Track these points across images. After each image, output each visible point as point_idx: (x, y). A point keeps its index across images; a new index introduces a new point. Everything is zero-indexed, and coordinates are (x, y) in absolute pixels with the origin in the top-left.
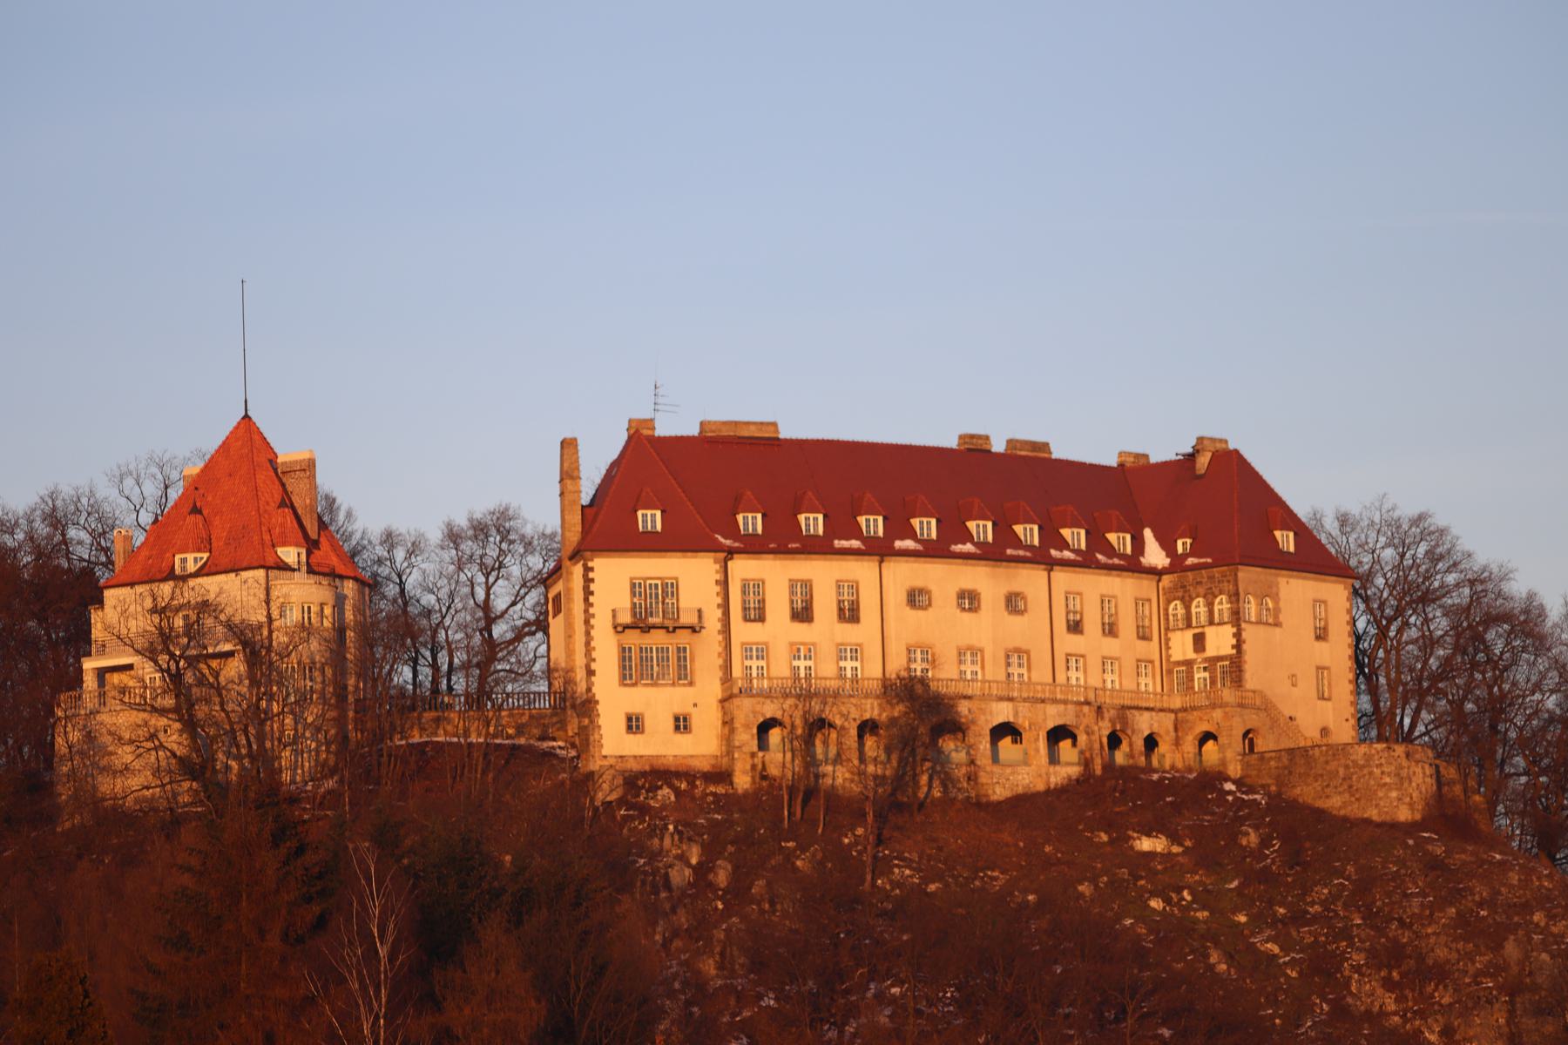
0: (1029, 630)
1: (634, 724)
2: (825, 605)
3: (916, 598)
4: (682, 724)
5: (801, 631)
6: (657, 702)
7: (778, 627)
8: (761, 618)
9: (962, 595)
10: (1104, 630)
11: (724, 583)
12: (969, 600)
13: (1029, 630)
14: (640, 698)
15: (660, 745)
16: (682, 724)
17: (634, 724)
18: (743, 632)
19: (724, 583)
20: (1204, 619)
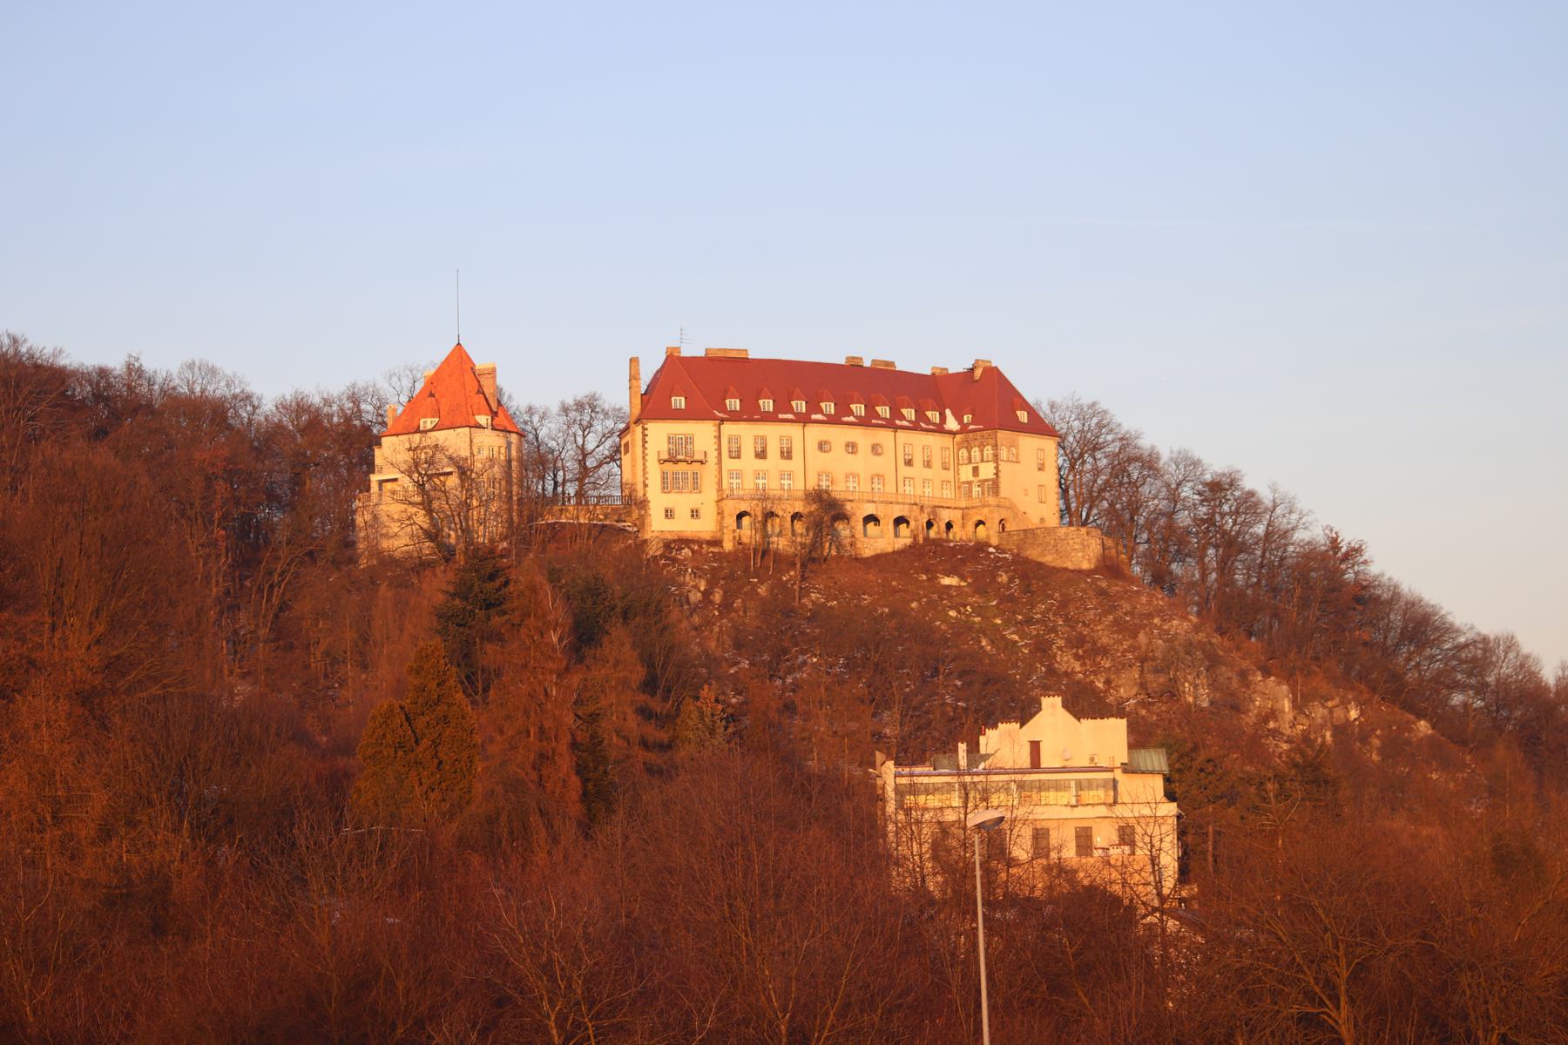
0: (884, 464)
1: (669, 514)
2: (773, 451)
3: (823, 446)
4: (695, 514)
6: (682, 502)
7: (748, 461)
10: (782, 452)
11: (719, 437)
12: (852, 448)
13: (884, 464)
14: (672, 500)
15: (683, 525)
16: (695, 514)
18: (728, 464)
19: (719, 437)
20: (978, 459)
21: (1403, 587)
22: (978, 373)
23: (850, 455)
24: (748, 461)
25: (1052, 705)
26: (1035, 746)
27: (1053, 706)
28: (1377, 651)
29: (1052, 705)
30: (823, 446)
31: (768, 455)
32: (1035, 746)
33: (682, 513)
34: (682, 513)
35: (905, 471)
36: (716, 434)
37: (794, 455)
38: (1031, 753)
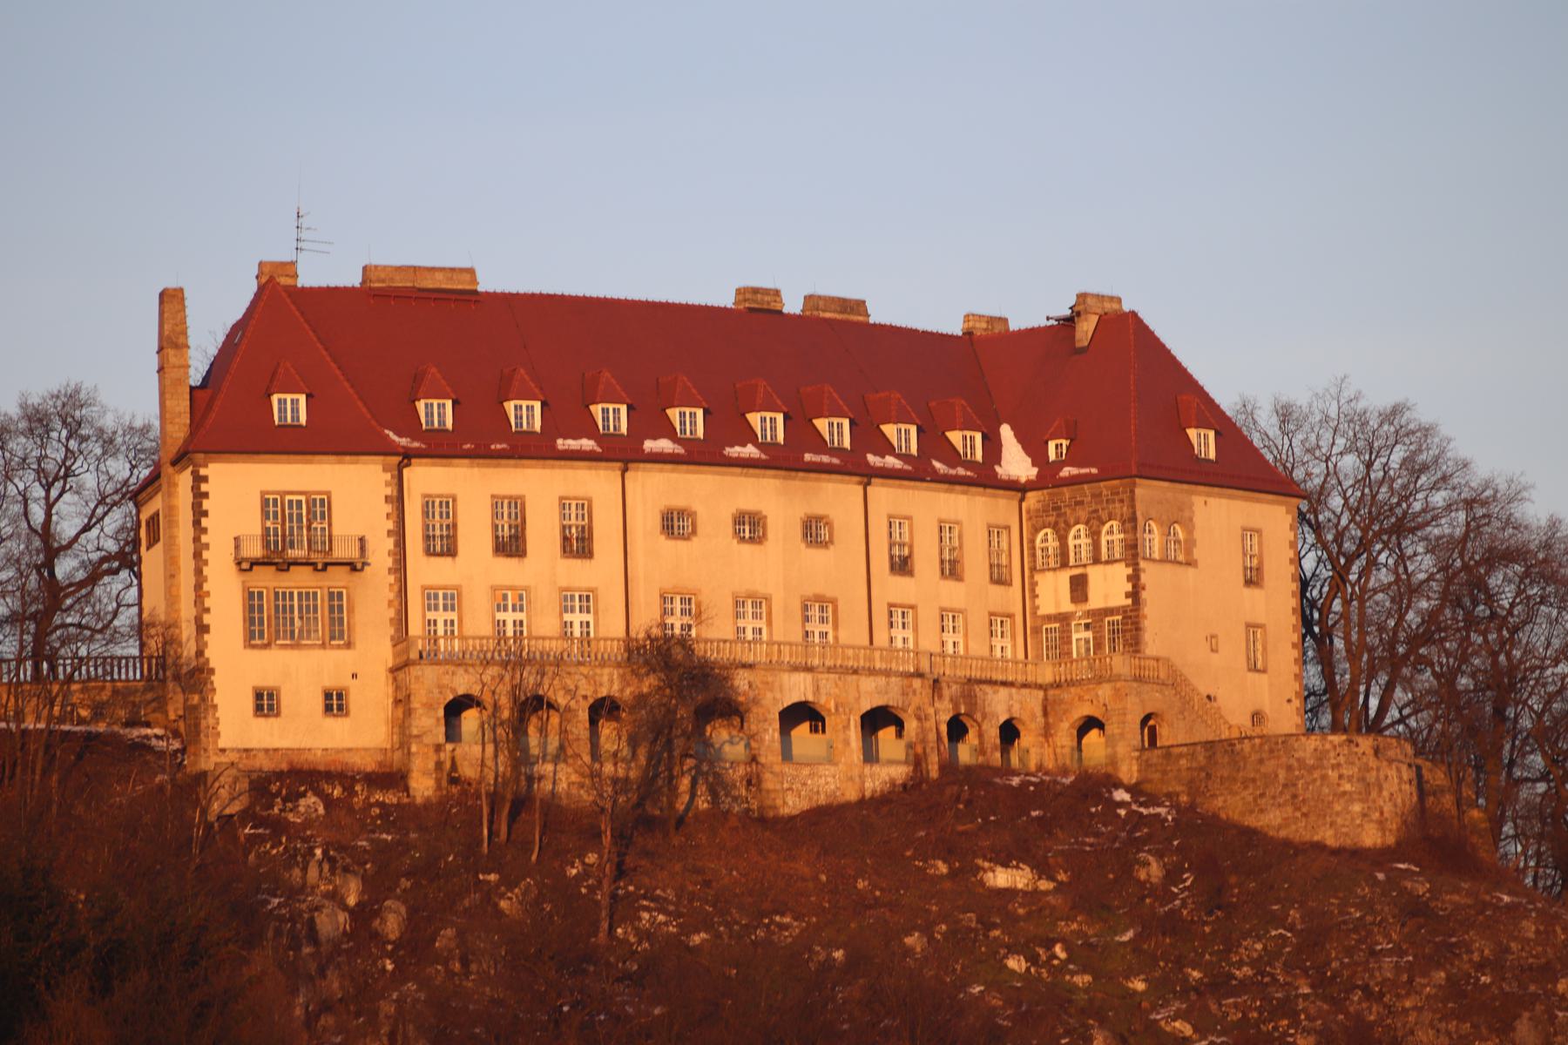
1: (265, 703)
2: (543, 533)
3: (675, 523)
5: (507, 571)
8: (451, 552)
9: (740, 519)
11: (398, 501)
12: (750, 527)
14: (272, 666)
16: (335, 702)
17: (265, 703)
18: (424, 571)
19: (398, 501)
30: (675, 523)
31: (531, 546)
33: (301, 700)
34: (301, 700)
35: (892, 588)
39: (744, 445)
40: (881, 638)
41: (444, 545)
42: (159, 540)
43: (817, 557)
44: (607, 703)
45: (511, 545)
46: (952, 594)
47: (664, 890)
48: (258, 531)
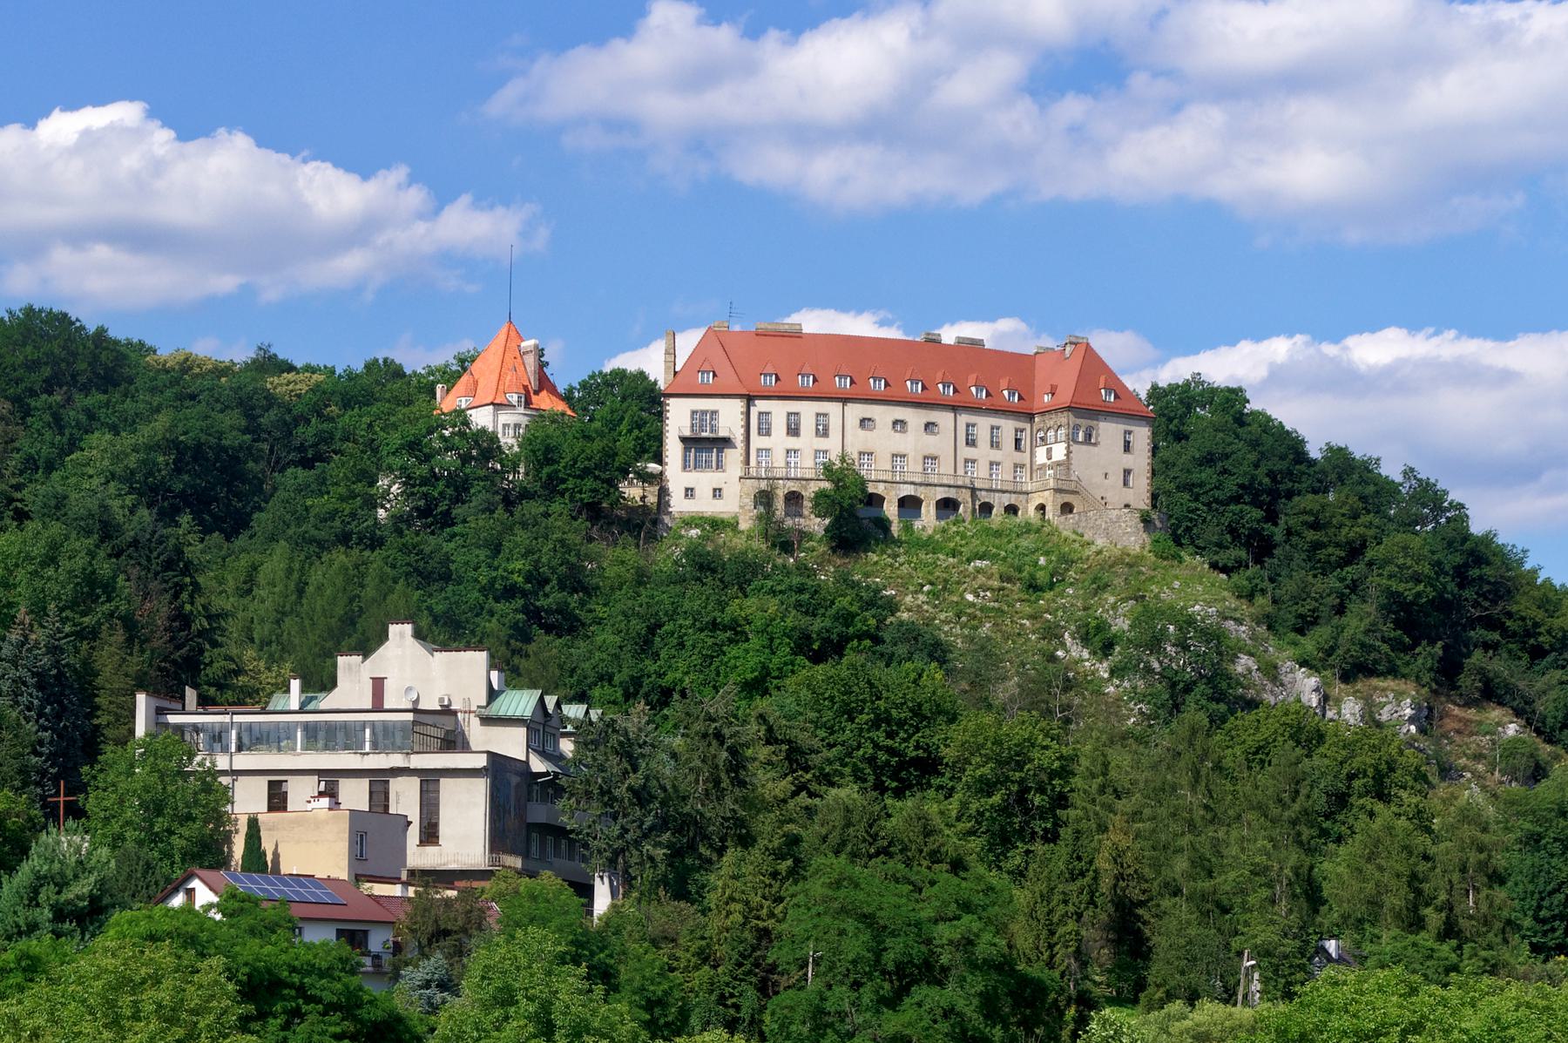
0: (940, 444)
1: (689, 493)
2: (807, 425)
3: (865, 422)
4: (717, 493)
5: (792, 442)
6: (704, 481)
7: (779, 439)
8: (768, 434)
9: (895, 423)
10: (817, 430)
12: (899, 424)
13: (940, 444)
15: (705, 505)
16: (717, 493)
17: (689, 493)
18: (757, 441)
21: (1308, 447)
22: (305, 153)
23: (898, 434)
24: (779, 439)
25: (400, 633)
26: (378, 684)
27: (402, 635)
28: (320, 588)
29: (400, 633)
30: (865, 422)
31: (802, 433)
32: (378, 684)
35: (966, 452)
36: (744, 410)
37: (831, 432)
38: (374, 695)
39: (960, 341)
40: (961, 471)
41: (765, 431)
42: (620, 375)
43: (930, 439)
44: (329, 686)
45: (793, 431)
46: (996, 455)
47: (1120, 653)
48: (689, 425)
